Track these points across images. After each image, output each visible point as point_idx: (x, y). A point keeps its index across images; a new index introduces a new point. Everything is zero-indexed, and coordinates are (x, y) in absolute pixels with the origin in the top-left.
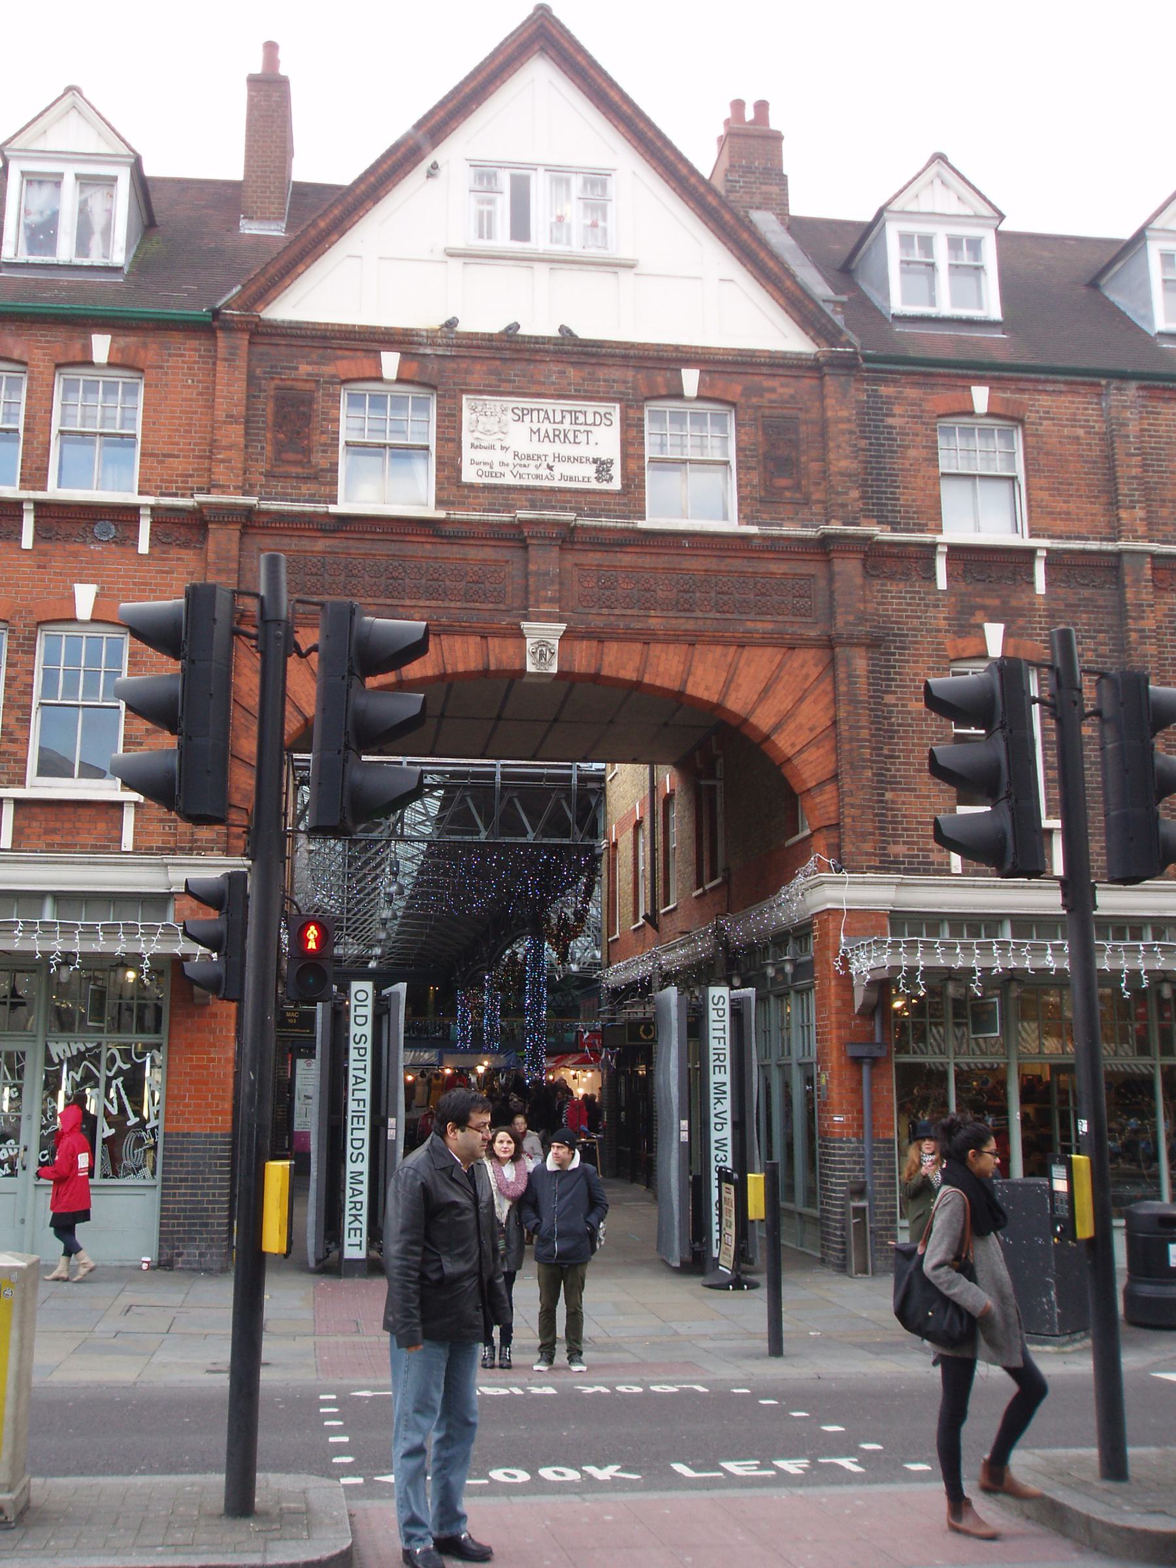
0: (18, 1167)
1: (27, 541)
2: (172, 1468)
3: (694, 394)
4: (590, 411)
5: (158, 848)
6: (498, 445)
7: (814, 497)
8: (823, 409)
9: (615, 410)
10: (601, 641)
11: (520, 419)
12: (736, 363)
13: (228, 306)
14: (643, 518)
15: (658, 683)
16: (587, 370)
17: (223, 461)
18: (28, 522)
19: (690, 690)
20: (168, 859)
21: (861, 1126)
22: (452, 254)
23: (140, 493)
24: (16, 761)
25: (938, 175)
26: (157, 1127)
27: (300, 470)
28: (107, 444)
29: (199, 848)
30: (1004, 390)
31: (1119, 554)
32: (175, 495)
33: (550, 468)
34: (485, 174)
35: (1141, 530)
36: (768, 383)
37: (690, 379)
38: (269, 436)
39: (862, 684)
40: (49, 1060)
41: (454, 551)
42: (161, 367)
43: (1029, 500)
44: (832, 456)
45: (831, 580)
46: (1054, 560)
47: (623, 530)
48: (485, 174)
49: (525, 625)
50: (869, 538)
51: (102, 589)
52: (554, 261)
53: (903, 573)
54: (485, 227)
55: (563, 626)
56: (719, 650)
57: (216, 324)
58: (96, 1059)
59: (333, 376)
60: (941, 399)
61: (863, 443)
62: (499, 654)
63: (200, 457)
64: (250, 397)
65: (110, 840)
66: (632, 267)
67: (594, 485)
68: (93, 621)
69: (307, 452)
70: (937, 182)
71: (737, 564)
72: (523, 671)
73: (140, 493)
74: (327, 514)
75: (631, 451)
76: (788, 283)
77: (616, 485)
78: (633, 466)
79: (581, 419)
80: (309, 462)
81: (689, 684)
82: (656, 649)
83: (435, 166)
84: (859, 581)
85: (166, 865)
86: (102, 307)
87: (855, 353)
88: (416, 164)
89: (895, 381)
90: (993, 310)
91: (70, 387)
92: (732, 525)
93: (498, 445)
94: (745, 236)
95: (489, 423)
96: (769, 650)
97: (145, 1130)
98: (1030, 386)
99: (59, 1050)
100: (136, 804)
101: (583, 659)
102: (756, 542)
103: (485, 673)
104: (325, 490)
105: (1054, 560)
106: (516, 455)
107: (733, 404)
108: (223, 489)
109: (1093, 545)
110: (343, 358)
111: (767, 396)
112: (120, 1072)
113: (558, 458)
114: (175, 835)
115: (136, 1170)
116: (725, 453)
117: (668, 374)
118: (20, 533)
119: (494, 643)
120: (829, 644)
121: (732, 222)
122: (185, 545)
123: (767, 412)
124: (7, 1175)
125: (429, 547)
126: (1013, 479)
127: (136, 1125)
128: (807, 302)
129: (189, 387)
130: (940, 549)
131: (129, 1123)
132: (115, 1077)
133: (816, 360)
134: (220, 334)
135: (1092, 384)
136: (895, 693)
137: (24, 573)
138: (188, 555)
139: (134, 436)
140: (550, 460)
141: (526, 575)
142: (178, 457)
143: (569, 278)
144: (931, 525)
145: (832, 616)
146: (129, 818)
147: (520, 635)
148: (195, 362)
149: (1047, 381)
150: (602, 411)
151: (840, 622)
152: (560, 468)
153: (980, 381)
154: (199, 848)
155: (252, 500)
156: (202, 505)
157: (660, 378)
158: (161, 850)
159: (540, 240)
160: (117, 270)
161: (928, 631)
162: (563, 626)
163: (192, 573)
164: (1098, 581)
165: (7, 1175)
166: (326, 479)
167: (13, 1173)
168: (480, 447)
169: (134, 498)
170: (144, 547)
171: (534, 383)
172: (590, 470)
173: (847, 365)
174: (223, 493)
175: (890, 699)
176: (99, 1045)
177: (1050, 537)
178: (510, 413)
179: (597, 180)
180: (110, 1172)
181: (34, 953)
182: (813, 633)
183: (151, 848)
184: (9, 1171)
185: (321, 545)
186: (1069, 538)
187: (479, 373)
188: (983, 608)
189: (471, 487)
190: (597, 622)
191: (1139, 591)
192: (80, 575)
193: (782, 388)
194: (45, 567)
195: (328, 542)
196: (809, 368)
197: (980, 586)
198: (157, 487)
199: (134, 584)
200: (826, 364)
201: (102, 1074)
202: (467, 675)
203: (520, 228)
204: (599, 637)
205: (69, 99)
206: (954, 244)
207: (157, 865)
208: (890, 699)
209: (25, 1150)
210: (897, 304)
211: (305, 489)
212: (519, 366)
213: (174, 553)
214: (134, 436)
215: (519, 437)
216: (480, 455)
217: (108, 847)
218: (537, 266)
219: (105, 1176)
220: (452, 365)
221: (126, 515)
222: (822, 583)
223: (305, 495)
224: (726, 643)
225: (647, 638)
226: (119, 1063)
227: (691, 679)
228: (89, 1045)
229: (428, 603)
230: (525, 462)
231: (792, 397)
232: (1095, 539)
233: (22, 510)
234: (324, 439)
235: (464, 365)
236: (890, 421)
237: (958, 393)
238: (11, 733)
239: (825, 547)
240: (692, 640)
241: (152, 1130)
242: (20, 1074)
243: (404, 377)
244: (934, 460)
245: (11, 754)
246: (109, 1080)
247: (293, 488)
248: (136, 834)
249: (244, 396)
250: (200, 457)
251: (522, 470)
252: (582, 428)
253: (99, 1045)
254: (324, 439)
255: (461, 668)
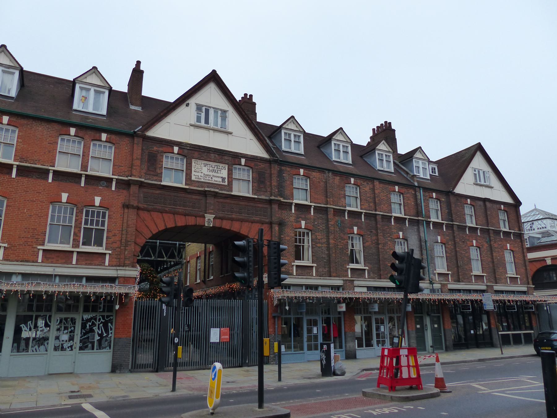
0: (73, 348)
1: (83, 185)
2: (195, 409)
3: (177, 153)
4: (221, 166)
5: (115, 265)
6: (200, 171)
7: (268, 190)
8: (271, 171)
9: (227, 166)
10: (222, 220)
11: (205, 166)
12: (251, 158)
13: (138, 131)
14: (232, 192)
15: (234, 230)
16: (221, 156)
17: (135, 169)
18: (83, 179)
19: (241, 232)
20: (118, 268)
21: (275, 332)
22: (191, 125)
23: (113, 175)
24: (78, 241)
25: (292, 121)
26: (111, 336)
27: (153, 173)
28: (4, 145)
29: (126, 265)
30: (306, 170)
31: (327, 208)
32: (122, 176)
33: (212, 178)
34: (199, 107)
35: (332, 203)
36: (259, 164)
37: (243, 161)
38: (146, 164)
39: (277, 232)
40: (83, 320)
41: (189, 196)
42: (120, 144)
43: (310, 195)
44: (272, 181)
45: (271, 209)
46: (315, 208)
47: (227, 194)
48: (199, 107)
49: (206, 215)
50: (280, 201)
51: (102, 198)
52: (215, 130)
53: (286, 209)
54: (199, 119)
55: (214, 216)
56: (248, 223)
57: (135, 135)
58: (96, 319)
59: (162, 151)
60: (294, 171)
61: (278, 179)
62: (199, 221)
63: (129, 167)
64: (142, 154)
65: (102, 263)
66: (231, 134)
67: (221, 183)
68: (66, 203)
69: (155, 169)
70: (292, 122)
71: (252, 204)
72: (204, 225)
73: (113, 175)
74: (160, 185)
75: (230, 176)
76: (265, 142)
77: (226, 184)
78: (230, 180)
79: (219, 168)
80: (156, 171)
81: (241, 231)
82: (234, 222)
83: (188, 104)
84: (277, 210)
85: (117, 270)
86: (7, 108)
87: (278, 159)
88: (184, 103)
89: (285, 166)
90: (302, 151)
91: (63, 140)
92: (250, 195)
93: (200, 171)
94: (256, 130)
95: (199, 166)
96: (258, 224)
97: (108, 337)
98: (311, 170)
99: (86, 317)
100: (110, 254)
101: (218, 224)
102: (256, 199)
103: (195, 226)
104: (159, 179)
105: (315, 208)
106: (204, 174)
107: (252, 168)
108: (135, 176)
109: (323, 206)
110: (165, 147)
111: (259, 167)
112: (102, 322)
113: (213, 176)
114: (119, 262)
115: (105, 348)
116: (183, 168)
117: (238, 159)
118: (81, 182)
119: (198, 218)
120: (271, 224)
121: (254, 127)
122: (124, 189)
123: (259, 170)
124: (70, 350)
125: (184, 194)
126: (307, 190)
127: (106, 336)
128: (269, 147)
129: (126, 149)
130: (83, 175)
131: (104, 336)
132: (101, 324)
133: (270, 160)
134: (135, 137)
135: (323, 171)
136: (283, 235)
137: (82, 192)
138: (125, 192)
139: (14, 145)
140: (212, 176)
141: (206, 203)
142: (123, 167)
143: (218, 135)
144: (291, 198)
145: (272, 217)
146: (107, 257)
147: (204, 217)
148: (129, 144)
149: (315, 170)
150: (224, 166)
151: (273, 219)
152: (214, 178)
153: (302, 168)
154: (126, 265)
155: (143, 180)
156: (130, 180)
157: (237, 160)
158: (115, 266)
159: (211, 124)
160: (12, 98)
161: (290, 222)
162: (214, 216)
163: (126, 196)
164: (323, 213)
165: (70, 350)
166: (159, 176)
167: (72, 350)
168: (196, 172)
169: (79, 172)
170: (113, 189)
171: (209, 158)
172: (220, 180)
173: (276, 161)
174: (135, 177)
175: (282, 236)
176: (96, 316)
177: (314, 203)
178: (203, 164)
179: (224, 112)
180: (98, 348)
181: (75, 292)
182: (267, 221)
183: (113, 265)
184: (70, 349)
185: (158, 192)
186: (318, 204)
187: (196, 154)
188: (301, 217)
189: (194, 181)
190: (221, 215)
191: (331, 216)
192: (96, 194)
193: (262, 165)
194: (87, 192)
195: (160, 191)
196: (268, 161)
197: (301, 212)
198: (117, 174)
199: (111, 198)
200: (273, 161)
201: (97, 323)
202: (192, 226)
203: (207, 121)
204: (222, 219)
205: (93, 70)
206: (295, 136)
207: (115, 269)
208: (282, 236)
209: (76, 343)
210: (334, 159)
211: (155, 178)
212: (206, 154)
213: (121, 191)
214: (14, 145)
215: (205, 170)
216: (196, 174)
217: (101, 264)
218: (210, 131)
219: (97, 349)
220: (190, 152)
221: (110, 180)
222: (269, 210)
223: (154, 179)
224: (249, 222)
225: (232, 220)
226: (102, 320)
227: (241, 230)
228: (94, 316)
229: (183, 208)
230: (206, 176)
231: (264, 167)
232: (323, 204)
233: (49, 172)
234: (159, 166)
235: (193, 152)
236: (284, 175)
237: (298, 170)
238: (76, 234)
239: (270, 202)
240: (242, 221)
241: (110, 337)
242: (75, 323)
243: (179, 153)
244: (292, 184)
245: (76, 239)
246: (99, 325)
247: (151, 177)
248: (109, 261)
249: (140, 153)
250: (129, 167)
251: (206, 178)
252: (219, 170)
253: (96, 316)
254: (159, 166)
255: (190, 224)
